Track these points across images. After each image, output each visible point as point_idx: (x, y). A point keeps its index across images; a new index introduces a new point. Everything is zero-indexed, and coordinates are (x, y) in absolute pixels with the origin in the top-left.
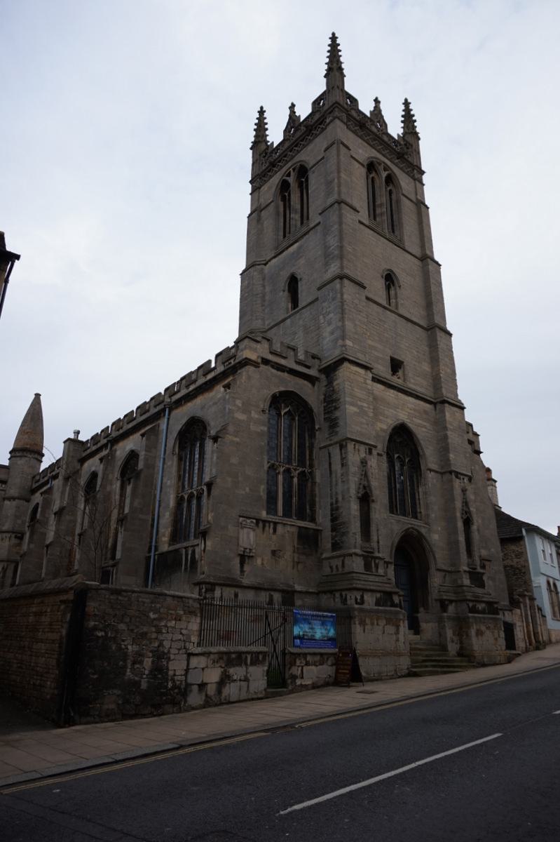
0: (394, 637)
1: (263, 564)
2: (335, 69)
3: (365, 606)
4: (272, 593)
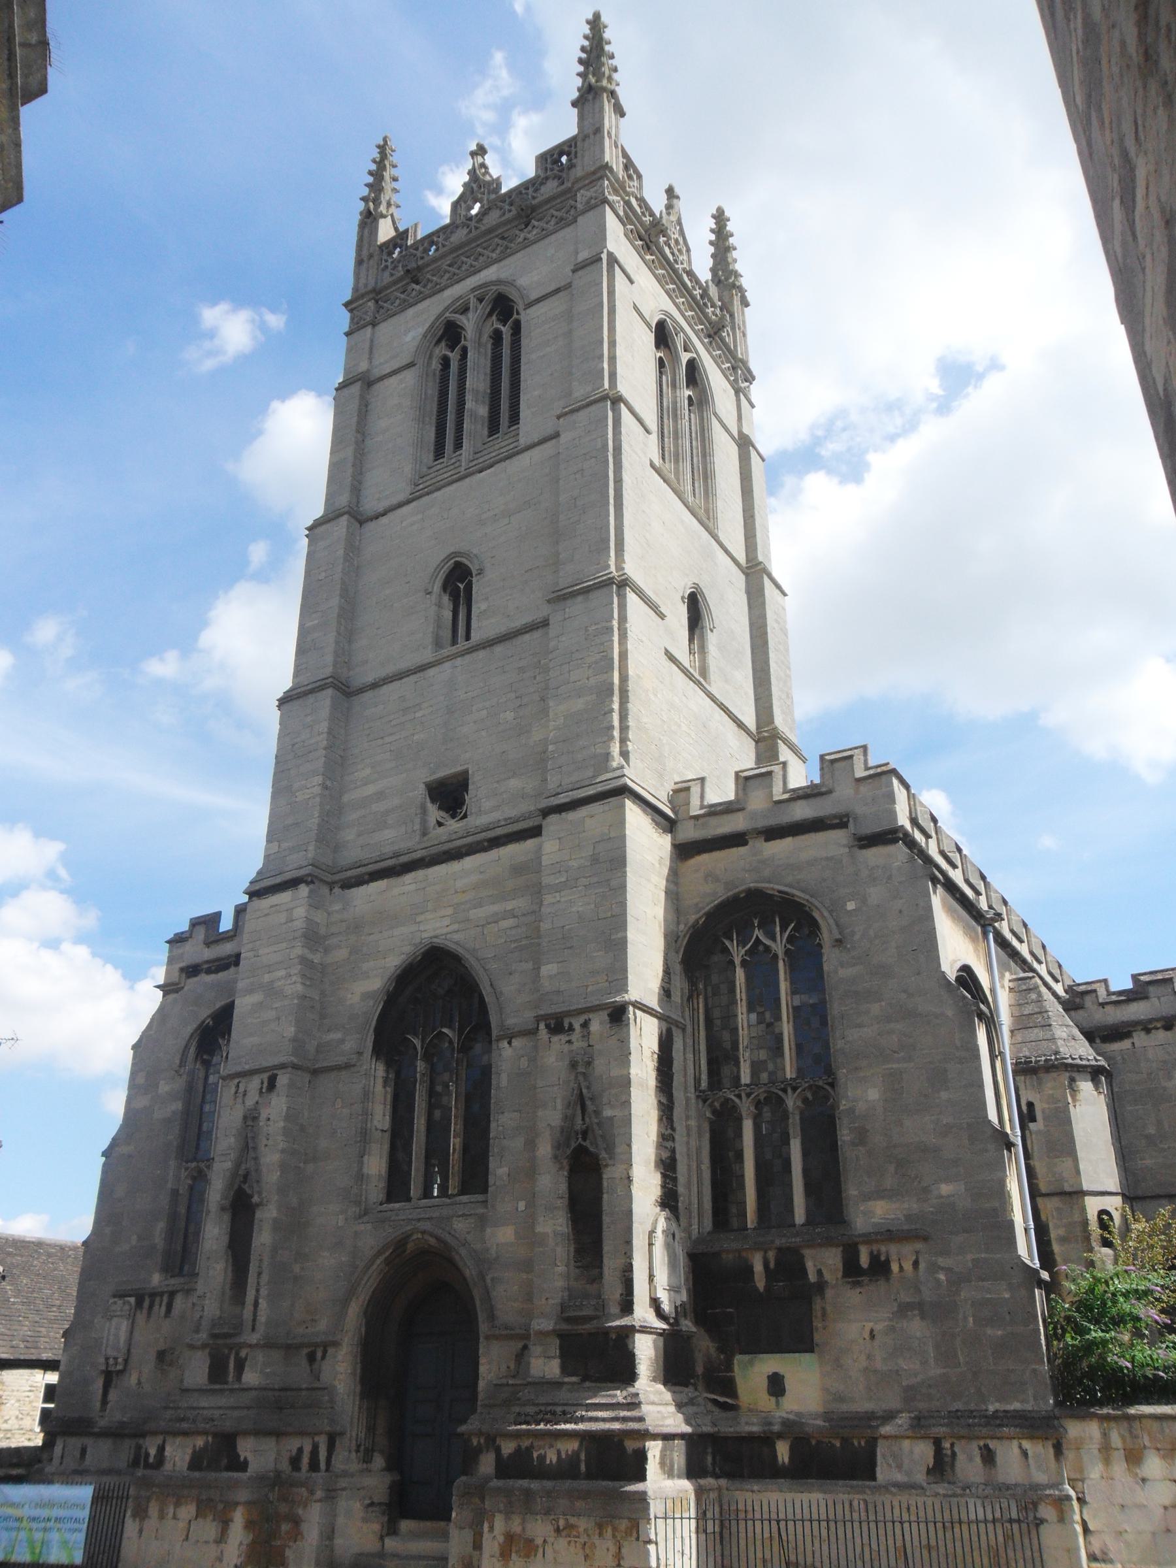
1: (139, 1383)
2: (595, 91)
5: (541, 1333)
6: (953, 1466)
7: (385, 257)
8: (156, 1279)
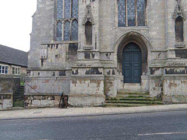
0: (96, 88)
1: (51, 61)
3: (79, 75)
4: (54, 71)
8: (52, 42)
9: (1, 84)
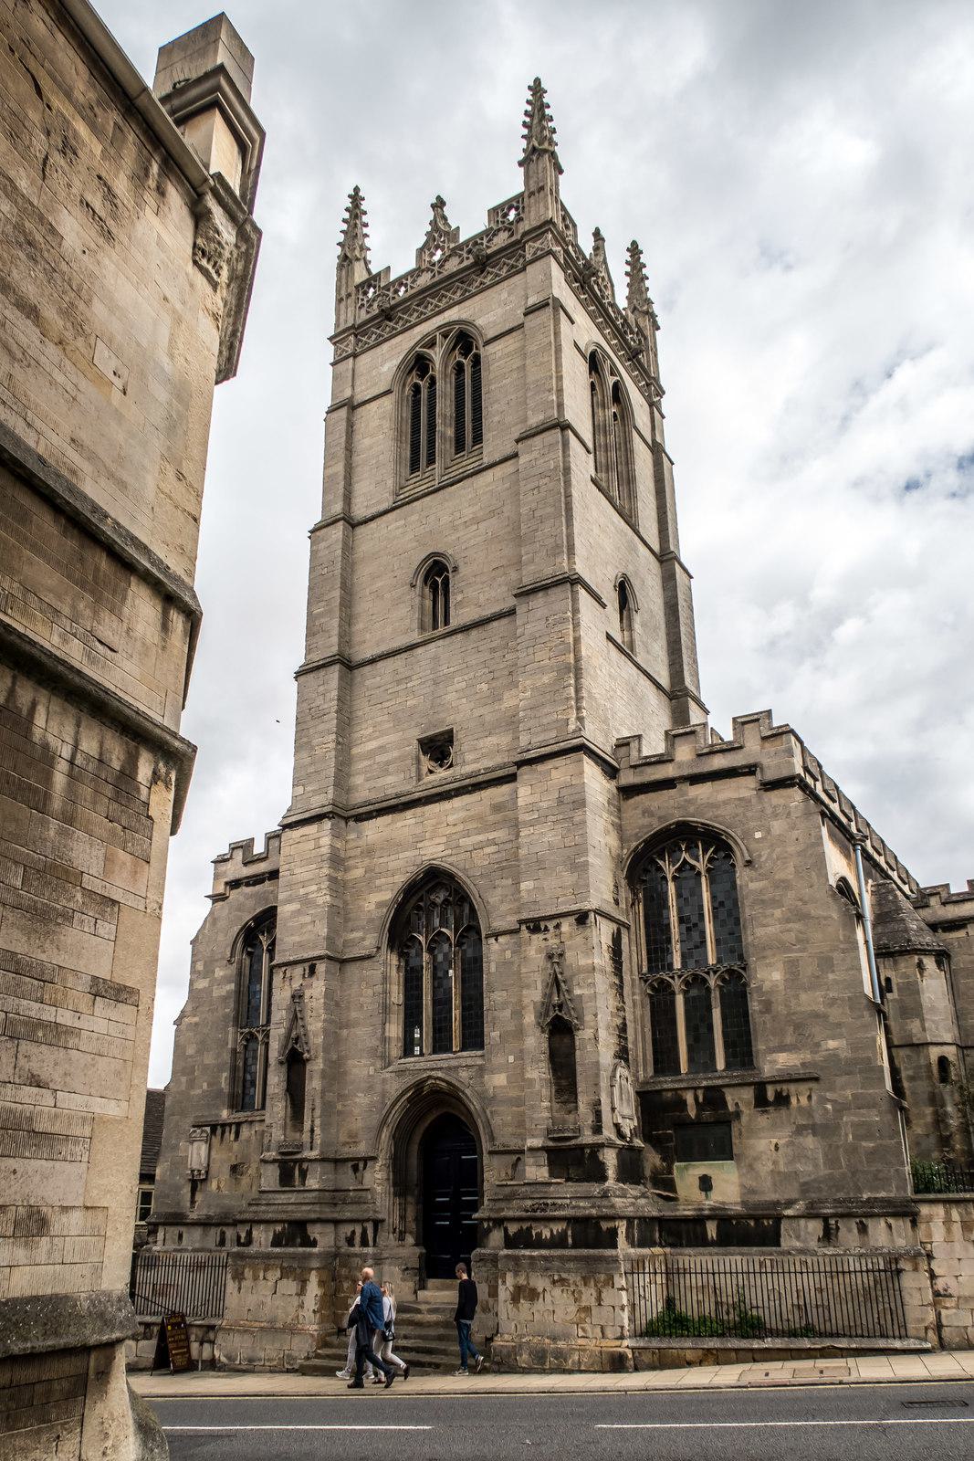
1: (219, 1188)
2: (540, 151)
4: (224, 1229)
5: (531, 1149)
6: (836, 1236)
7: (361, 297)
8: (225, 1114)
9: (972, 1090)
